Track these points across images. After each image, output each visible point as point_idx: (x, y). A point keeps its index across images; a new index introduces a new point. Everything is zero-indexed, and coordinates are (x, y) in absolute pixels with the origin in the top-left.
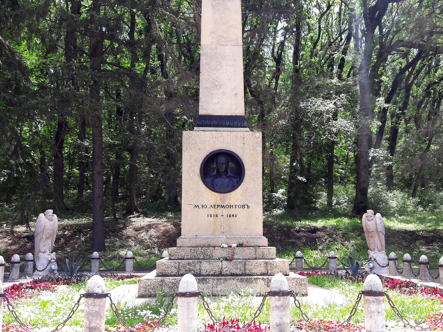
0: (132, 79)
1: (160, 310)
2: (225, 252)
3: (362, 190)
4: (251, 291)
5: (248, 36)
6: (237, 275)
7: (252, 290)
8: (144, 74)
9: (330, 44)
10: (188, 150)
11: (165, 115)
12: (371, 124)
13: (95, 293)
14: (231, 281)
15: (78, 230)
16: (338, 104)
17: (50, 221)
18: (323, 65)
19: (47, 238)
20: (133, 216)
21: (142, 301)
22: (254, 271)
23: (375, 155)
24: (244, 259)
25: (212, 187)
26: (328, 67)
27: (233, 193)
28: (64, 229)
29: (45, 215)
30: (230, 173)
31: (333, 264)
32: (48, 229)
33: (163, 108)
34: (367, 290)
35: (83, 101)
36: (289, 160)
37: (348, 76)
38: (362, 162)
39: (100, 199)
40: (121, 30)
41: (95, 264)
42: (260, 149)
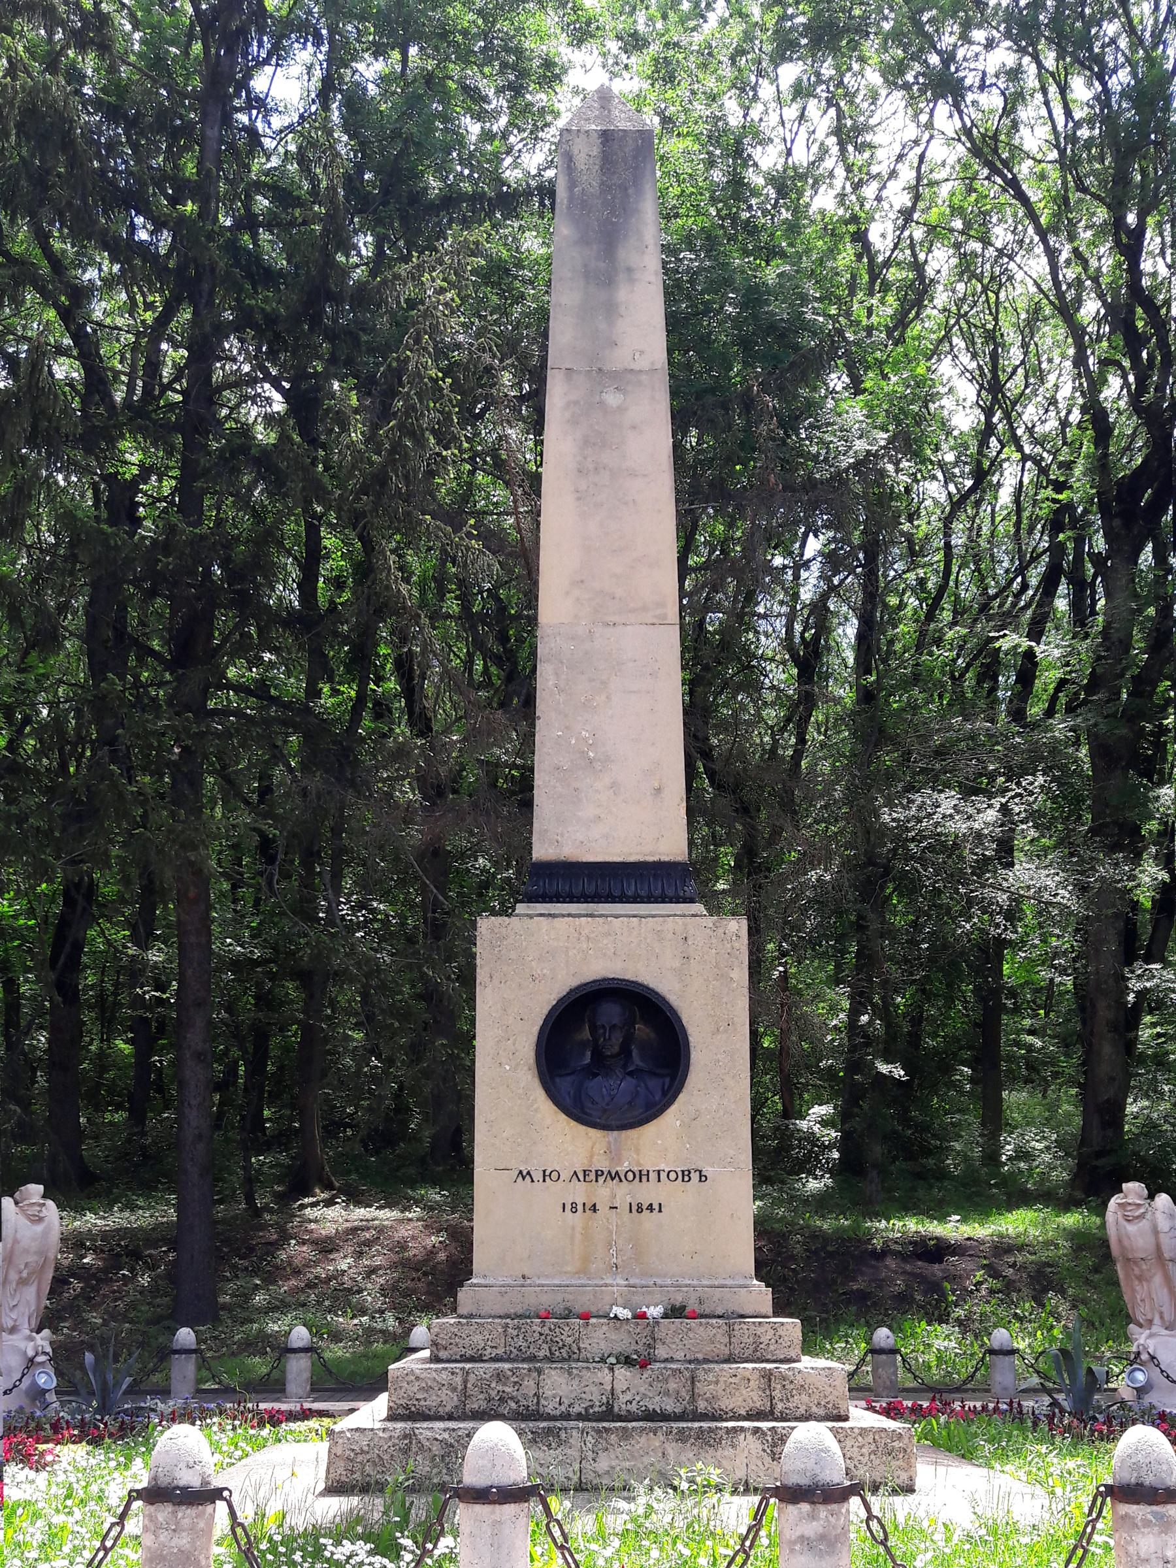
0: (309, 738)
1: (401, 1541)
2: (624, 1335)
3: (1104, 1112)
4: (715, 1474)
5: (697, 590)
6: (664, 1417)
7: (718, 1471)
8: (351, 720)
9: (984, 608)
10: (496, 981)
11: (420, 859)
12: (1132, 878)
13: (177, 1488)
14: (643, 1440)
15: (124, 1250)
16: (1017, 809)
17: (32, 1221)
18: (962, 675)
19: (23, 1282)
20: (312, 1200)
21: (334, 1507)
22: (726, 1403)
23: (1148, 985)
24: (690, 1362)
25: (578, 1108)
26: (979, 682)
27: (651, 1129)
28: (83, 1245)
29: (16, 1203)
30: (637, 1060)
31: (1003, 1376)
32: (26, 1251)
33: (415, 834)
34: (1124, 1481)
35: (145, 816)
36: (846, 1004)
37: (1050, 713)
38: (1104, 1012)
39: (201, 1146)
40: (271, 574)
41: (184, 1371)
42: (740, 975)
